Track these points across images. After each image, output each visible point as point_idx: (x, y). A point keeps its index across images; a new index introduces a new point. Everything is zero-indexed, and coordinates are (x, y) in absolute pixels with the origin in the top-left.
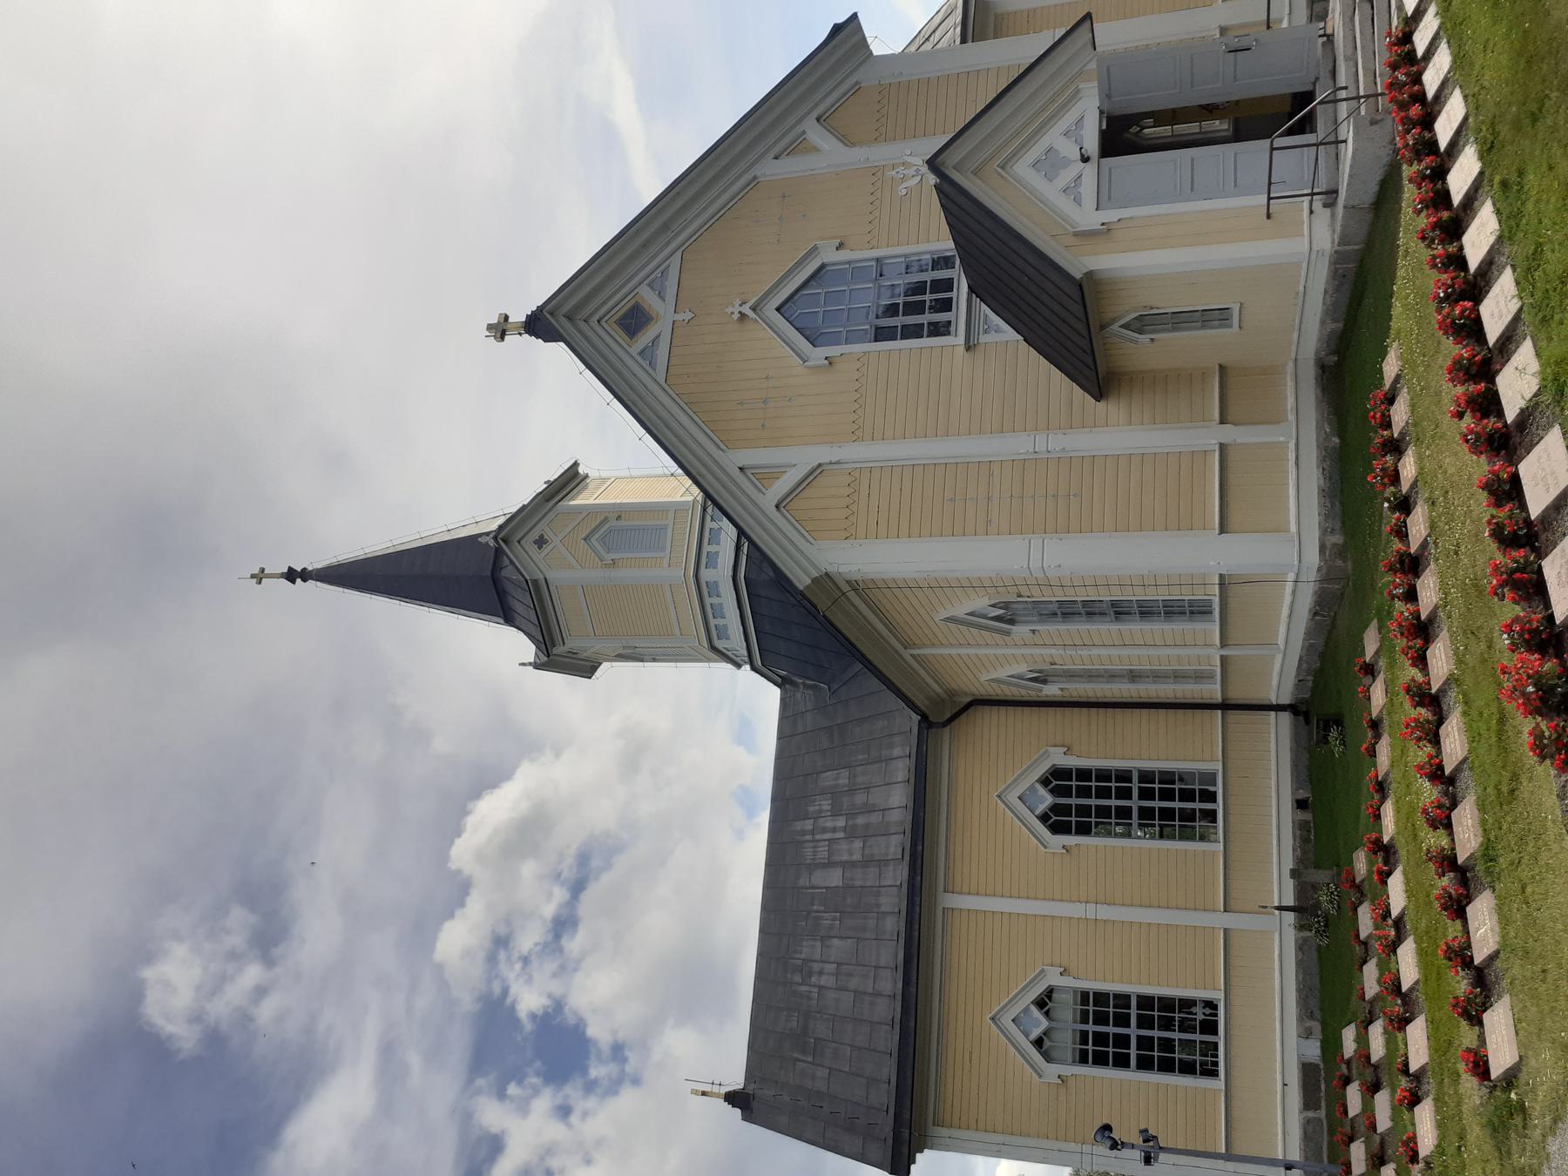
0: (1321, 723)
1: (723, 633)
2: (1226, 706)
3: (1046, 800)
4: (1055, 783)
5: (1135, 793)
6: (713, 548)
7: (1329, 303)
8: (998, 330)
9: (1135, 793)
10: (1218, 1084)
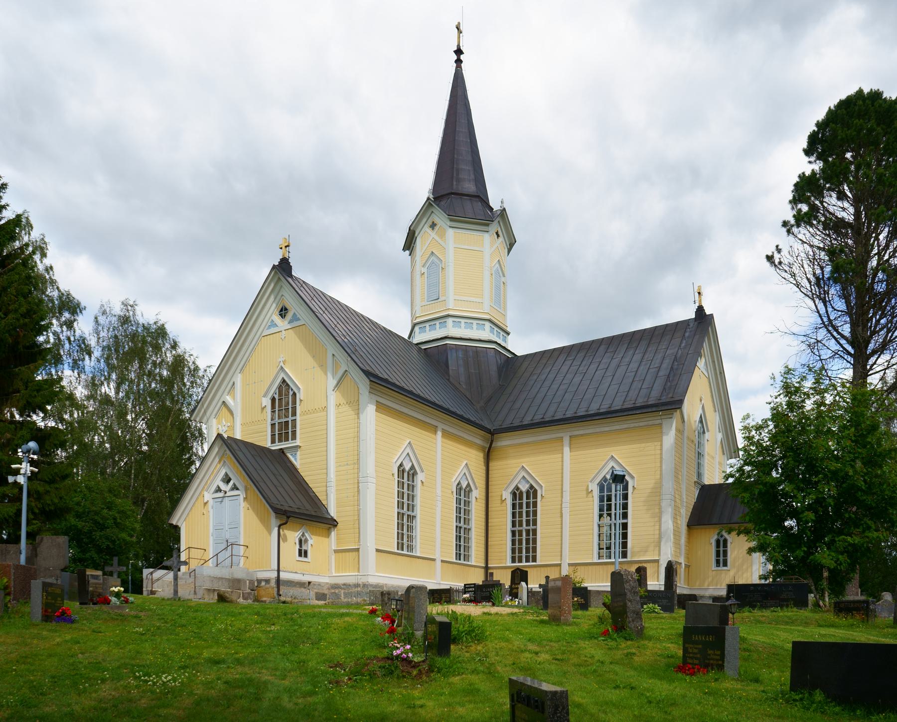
1: (423, 330)
3: (524, 488)
4: (605, 484)
5: (528, 528)
6: (463, 325)
9: (528, 528)
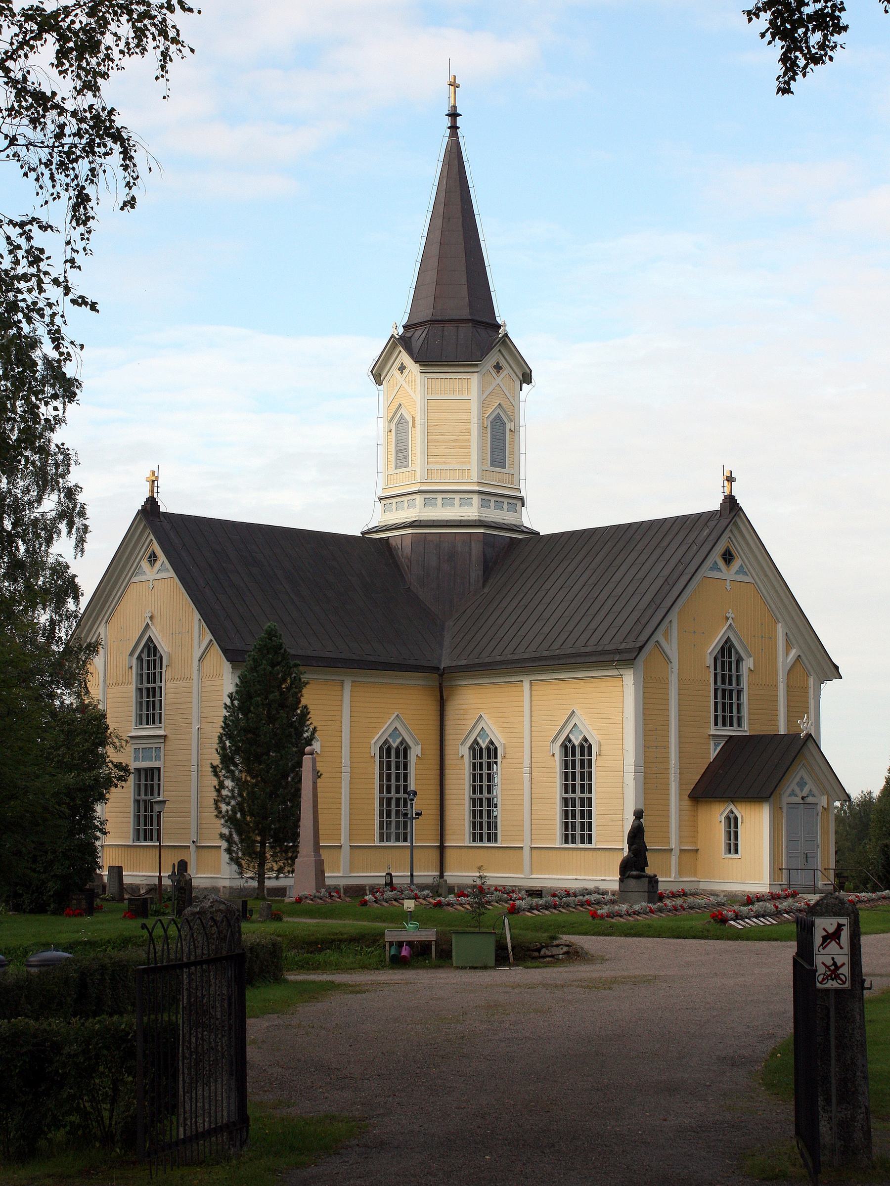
0: (540, 892)
2: (442, 849)
7: (737, 893)
8: (715, 750)
10: (558, 843)
